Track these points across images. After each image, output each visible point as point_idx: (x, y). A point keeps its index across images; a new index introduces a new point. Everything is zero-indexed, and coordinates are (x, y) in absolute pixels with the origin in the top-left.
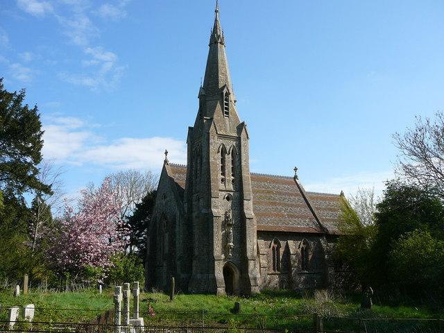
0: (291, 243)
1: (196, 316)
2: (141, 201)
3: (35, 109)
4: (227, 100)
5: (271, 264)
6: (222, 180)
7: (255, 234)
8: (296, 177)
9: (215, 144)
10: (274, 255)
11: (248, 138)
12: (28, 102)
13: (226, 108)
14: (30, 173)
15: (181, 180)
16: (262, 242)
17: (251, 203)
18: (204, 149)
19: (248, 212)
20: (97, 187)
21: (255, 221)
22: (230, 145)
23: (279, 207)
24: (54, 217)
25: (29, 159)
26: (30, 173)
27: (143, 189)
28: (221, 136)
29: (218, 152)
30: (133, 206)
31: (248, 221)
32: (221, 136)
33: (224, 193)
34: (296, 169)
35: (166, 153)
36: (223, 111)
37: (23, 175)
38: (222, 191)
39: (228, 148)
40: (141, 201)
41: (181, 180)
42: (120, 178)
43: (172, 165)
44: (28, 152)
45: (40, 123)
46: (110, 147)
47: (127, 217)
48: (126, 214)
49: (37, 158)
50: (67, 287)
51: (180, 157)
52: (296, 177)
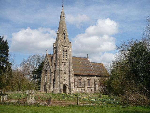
1: (126, 102)
2: (40, 64)
3: (6, 41)
7: (73, 76)
12: (5, 39)
14: (5, 60)
16: (75, 77)
20: (26, 59)
21: (73, 71)
24: (12, 71)
25: (5, 56)
26: (5, 60)
27: (41, 60)
30: (38, 66)
34: (88, 55)
35: (47, 51)
37: (4, 60)
40: (40, 64)
42: (33, 57)
43: (49, 54)
44: (4, 53)
45: (8, 46)
46: (36, 30)
47: (36, 70)
48: (36, 69)
49: (7, 55)
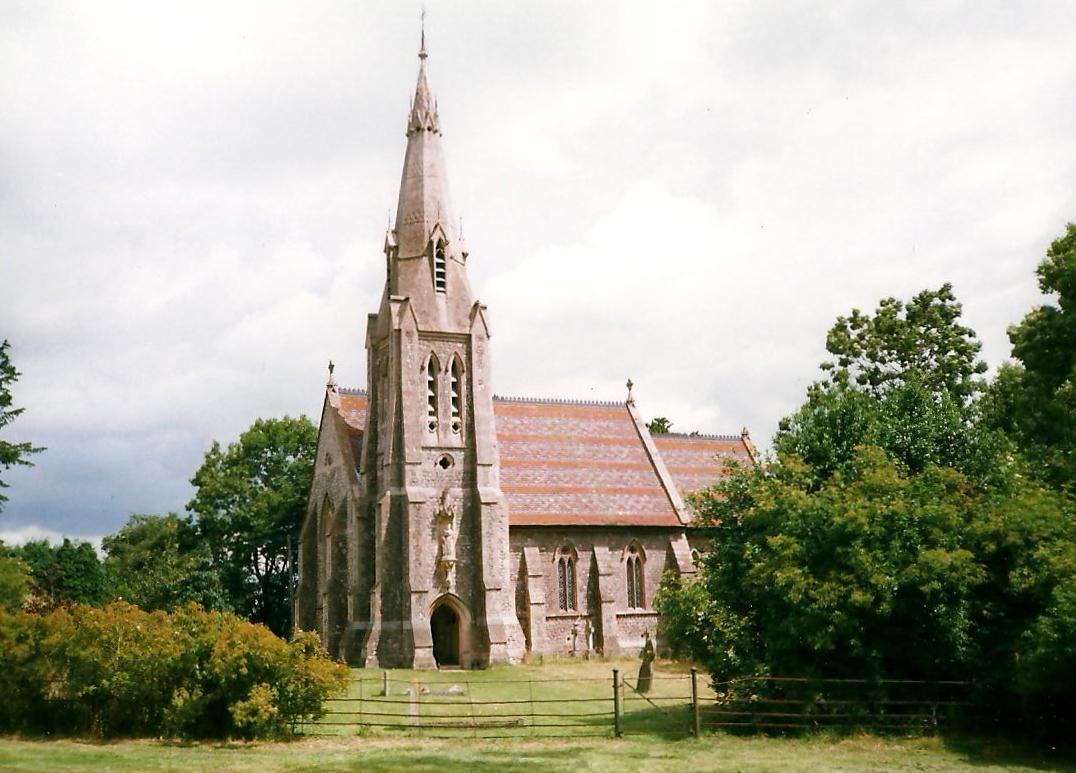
0: (602, 552)
4: (440, 255)
5: (557, 598)
6: (432, 426)
7: (508, 530)
8: (630, 402)
9: (414, 354)
10: (563, 577)
11: (488, 337)
13: (440, 265)
15: (358, 419)
17: (495, 470)
18: (393, 365)
19: (489, 489)
22: (447, 353)
23: (581, 472)
28: (425, 335)
29: (423, 368)
31: (484, 510)
32: (425, 335)
33: (438, 453)
36: (432, 270)
38: (430, 448)
39: (442, 356)
41: (358, 419)
43: (343, 392)
50: (634, 562)
51: (355, 375)
52: (630, 402)
